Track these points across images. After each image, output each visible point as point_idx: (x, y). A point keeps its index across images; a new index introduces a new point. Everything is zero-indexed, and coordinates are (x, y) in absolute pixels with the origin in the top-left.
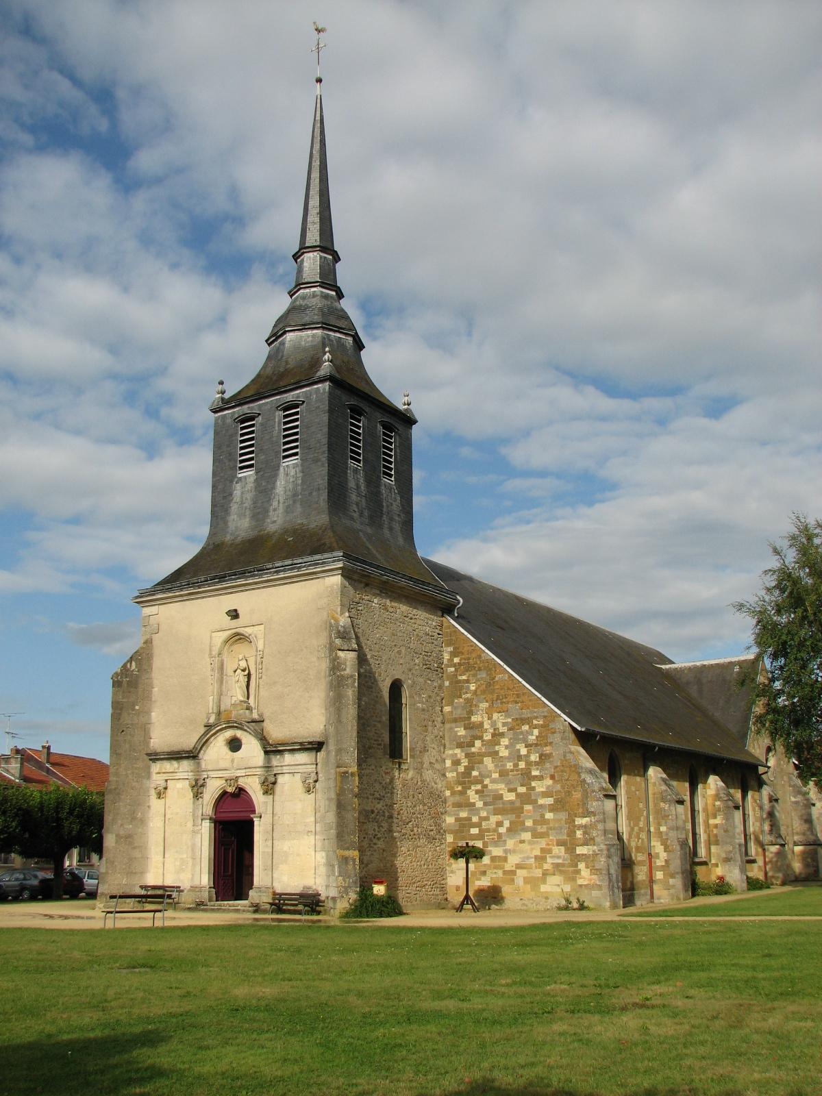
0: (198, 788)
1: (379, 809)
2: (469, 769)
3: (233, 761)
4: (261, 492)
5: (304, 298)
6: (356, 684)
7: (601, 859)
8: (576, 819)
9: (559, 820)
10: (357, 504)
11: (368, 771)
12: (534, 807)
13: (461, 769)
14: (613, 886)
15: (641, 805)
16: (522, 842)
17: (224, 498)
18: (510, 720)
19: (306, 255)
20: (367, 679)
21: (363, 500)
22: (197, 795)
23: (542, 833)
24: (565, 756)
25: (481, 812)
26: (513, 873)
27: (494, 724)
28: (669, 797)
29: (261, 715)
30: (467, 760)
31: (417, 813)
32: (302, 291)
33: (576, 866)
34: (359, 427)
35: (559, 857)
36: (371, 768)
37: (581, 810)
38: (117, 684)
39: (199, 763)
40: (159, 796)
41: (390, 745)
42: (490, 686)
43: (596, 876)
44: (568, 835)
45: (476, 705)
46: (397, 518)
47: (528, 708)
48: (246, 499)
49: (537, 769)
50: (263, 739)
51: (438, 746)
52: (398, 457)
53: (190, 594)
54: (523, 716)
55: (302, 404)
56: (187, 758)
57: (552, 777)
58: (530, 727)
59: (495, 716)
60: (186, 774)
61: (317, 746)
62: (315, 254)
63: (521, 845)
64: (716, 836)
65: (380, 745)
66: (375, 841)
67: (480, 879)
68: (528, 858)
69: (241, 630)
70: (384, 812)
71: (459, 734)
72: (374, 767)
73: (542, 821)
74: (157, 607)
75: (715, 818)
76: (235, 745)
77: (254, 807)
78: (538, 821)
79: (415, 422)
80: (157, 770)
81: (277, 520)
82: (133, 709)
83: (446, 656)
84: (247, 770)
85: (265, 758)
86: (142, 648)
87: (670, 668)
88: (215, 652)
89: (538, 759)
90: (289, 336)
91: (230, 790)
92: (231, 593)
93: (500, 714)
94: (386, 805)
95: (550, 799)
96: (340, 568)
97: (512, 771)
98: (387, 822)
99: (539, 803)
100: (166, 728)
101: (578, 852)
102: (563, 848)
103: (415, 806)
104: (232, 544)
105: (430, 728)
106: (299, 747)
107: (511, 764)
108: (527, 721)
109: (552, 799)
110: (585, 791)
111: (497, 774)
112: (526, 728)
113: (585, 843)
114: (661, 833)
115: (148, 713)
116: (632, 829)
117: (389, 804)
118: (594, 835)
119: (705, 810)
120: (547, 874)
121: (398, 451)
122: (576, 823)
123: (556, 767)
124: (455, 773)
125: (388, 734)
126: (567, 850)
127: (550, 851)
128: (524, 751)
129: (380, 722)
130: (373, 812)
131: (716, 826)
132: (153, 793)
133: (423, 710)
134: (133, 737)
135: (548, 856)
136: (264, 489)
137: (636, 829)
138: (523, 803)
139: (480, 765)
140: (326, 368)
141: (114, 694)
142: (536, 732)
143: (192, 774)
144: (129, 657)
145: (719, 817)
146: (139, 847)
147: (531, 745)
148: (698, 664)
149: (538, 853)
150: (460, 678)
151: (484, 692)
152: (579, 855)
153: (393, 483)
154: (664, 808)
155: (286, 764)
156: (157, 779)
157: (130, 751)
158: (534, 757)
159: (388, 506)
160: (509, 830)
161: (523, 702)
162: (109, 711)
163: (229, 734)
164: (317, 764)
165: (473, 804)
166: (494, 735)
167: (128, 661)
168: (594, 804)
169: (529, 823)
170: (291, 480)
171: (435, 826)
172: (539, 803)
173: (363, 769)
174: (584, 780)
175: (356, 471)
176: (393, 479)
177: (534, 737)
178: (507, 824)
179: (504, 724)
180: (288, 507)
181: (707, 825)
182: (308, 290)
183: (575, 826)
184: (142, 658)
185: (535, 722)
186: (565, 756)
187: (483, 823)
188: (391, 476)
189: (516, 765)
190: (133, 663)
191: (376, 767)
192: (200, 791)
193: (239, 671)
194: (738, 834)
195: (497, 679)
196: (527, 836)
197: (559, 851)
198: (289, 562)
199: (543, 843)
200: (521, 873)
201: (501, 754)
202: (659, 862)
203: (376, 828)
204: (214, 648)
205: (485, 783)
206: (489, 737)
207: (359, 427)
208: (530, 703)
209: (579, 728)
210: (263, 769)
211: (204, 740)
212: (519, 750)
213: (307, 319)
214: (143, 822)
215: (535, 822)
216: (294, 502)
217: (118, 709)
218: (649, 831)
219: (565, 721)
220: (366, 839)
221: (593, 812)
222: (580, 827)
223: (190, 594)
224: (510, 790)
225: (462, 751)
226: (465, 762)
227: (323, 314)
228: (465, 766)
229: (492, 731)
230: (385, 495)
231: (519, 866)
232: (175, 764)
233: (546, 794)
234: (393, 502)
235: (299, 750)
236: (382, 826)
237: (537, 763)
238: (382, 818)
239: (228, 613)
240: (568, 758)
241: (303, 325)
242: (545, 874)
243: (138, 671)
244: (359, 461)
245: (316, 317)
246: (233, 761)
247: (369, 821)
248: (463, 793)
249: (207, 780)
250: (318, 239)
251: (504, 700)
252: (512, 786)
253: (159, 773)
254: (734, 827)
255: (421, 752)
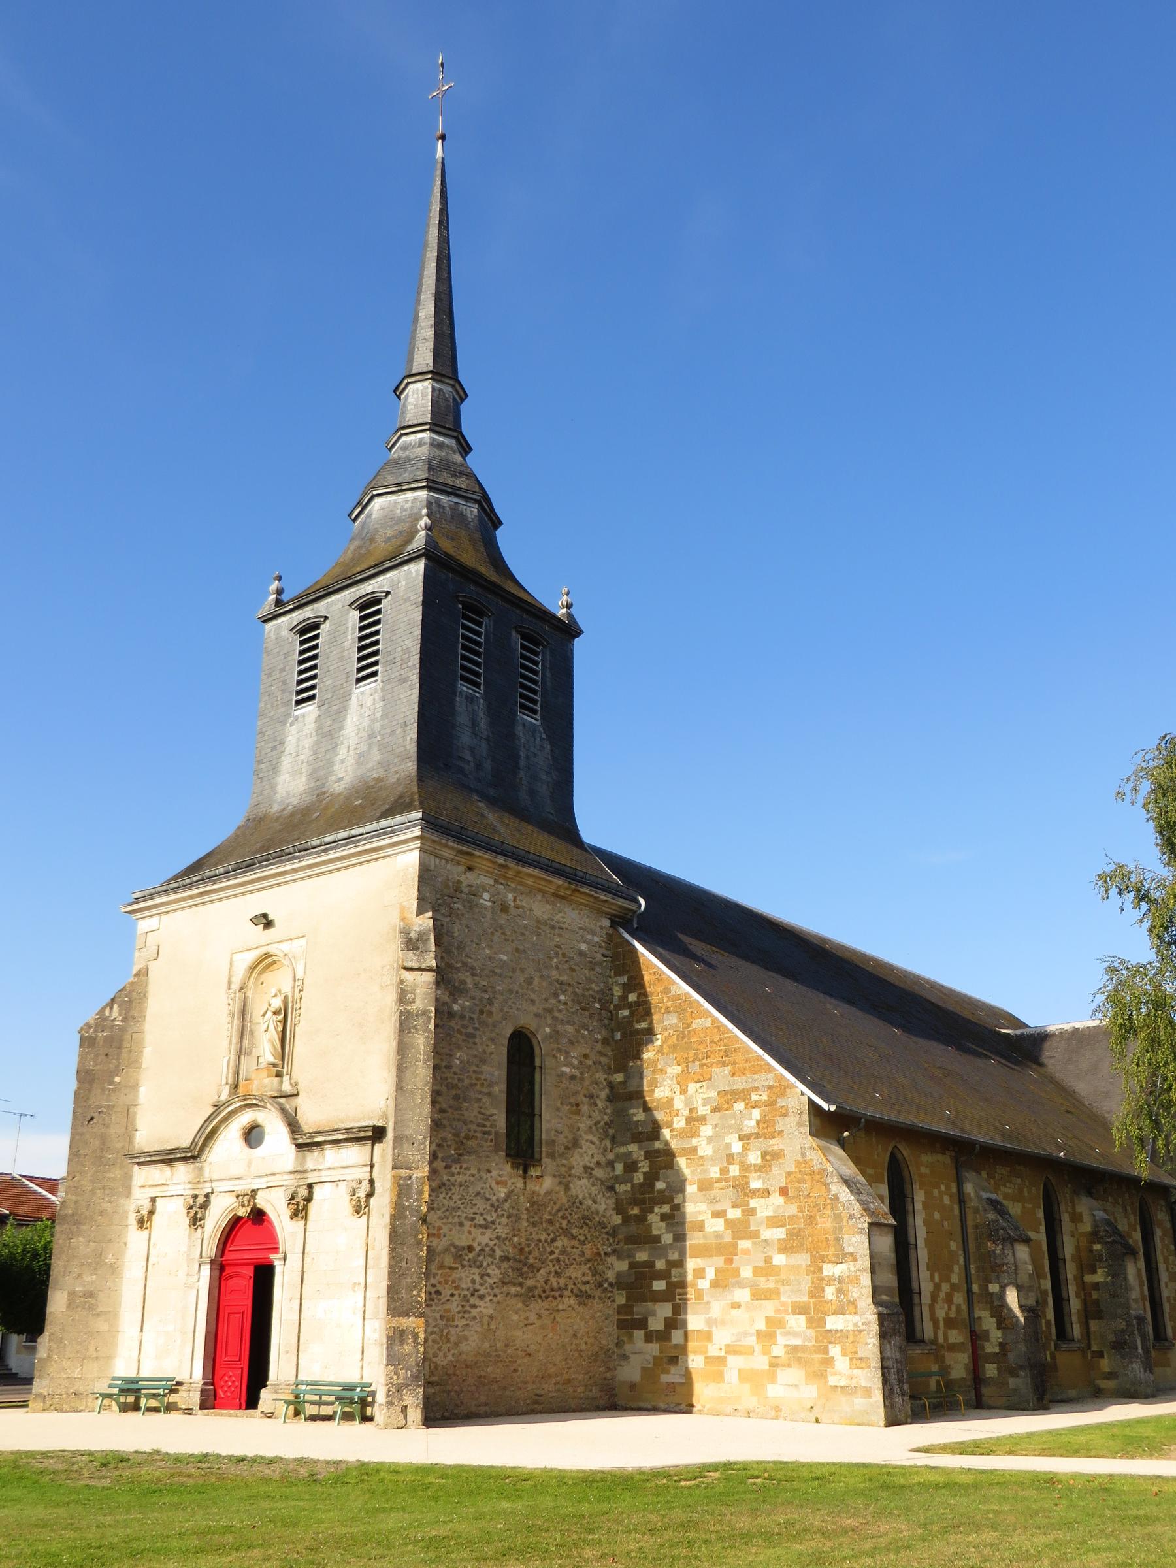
0: (197, 1213)
1: (483, 1244)
2: (651, 1178)
3: (249, 1164)
4: (324, 735)
5: (405, 448)
6: (432, 1026)
7: (869, 1341)
8: (825, 1266)
9: (795, 1268)
10: (472, 750)
11: (460, 1178)
12: (754, 1243)
13: (639, 1178)
14: (891, 1391)
15: (953, 1246)
16: (736, 1306)
17: (274, 748)
18: (714, 1094)
19: (411, 386)
20: (466, 1022)
21: (484, 745)
22: (196, 1221)
23: (769, 1290)
24: (803, 1155)
25: (670, 1252)
26: (721, 1360)
27: (688, 1102)
28: (1001, 1232)
29: (294, 1085)
30: (647, 1163)
31: (557, 1252)
32: (404, 439)
33: (826, 1350)
34: (479, 634)
35: (796, 1335)
36: (469, 1173)
37: (831, 1251)
38: (87, 1041)
39: (201, 1169)
40: (141, 1223)
41: (508, 1135)
42: (683, 1038)
43: (859, 1371)
44: (812, 1295)
45: (661, 1070)
46: (544, 777)
47: (743, 1074)
48: (304, 748)
49: (759, 1177)
50: (293, 1126)
51: (601, 1140)
52: (549, 684)
53: (202, 894)
54: (735, 1087)
55: (386, 596)
56: (185, 1159)
57: (784, 1192)
58: (747, 1105)
59: (692, 1087)
60: (182, 1187)
61: (377, 1134)
62: (426, 383)
63: (734, 1312)
64: (1096, 1302)
65: (489, 1133)
66: (473, 1301)
67: (668, 1372)
68: (746, 1334)
69: (272, 949)
70: (493, 1251)
71: (635, 1119)
72: (475, 1172)
73: (768, 1269)
74: (157, 918)
75: (1094, 1272)
76: (252, 1135)
77: (277, 1243)
78: (761, 1268)
79: (579, 633)
80: (140, 1184)
81: (345, 772)
82: (111, 1082)
83: (617, 991)
84: (270, 1178)
85: (297, 1157)
86: (132, 983)
87: (1023, 1034)
88: (235, 986)
89: (759, 1161)
90: (377, 503)
91: (243, 1212)
92: (262, 889)
93: (699, 1085)
94: (498, 1238)
95: (781, 1229)
96: (417, 838)
97: (718, 1181)
98: (499, 1268)
99: (763, 1237)
100: (161, 1108)
101: (828, 1327)
102: (803, 1318)
103: (553, 1240)
104: (278, 818)
105: (585, 1108)
106: (345, 1136)
107: (717, 1169)
108: (742, 1095)
109: (783, 1230)
110: (837, 1217)
111: (695, 1187)
112: (740, 1106)
113: (840, 1311)
114: (992, 1294)
115: (135, 1087)
116: (937, 1287)
117: (504, 1236)
118: (855, 1295)
119: (1077, 1258)
120: (777, 1365)
121: (548, 674)
122: (825, 1273)
123: (789, 1174)
124: (629, 1185)
125: (504, 1115)
126: (810, 1321)
127: (781, 1323)
128: (737, 1147)
129: (489, 1094)
130: (470, 1249)
131: (1096, 1286)
132: (132, 1220)
133: (573, 1077)
134: (108, 1127)
135: (778, 1331)
136: (328, 735)
137: (945, 1287)
138: (737, 1236)
139: (669, 1172)
140: (419, 541)
141: (83, 1058)
142: (756, 1114)
143: (190, 1186)
144: (108, 1000)
145: (1100, 1271)
146: (106, 1313)
147: (748, 1137)
148: (1067, 1027)
149: (761, 1325)
150: (637, 1026)
151: (674, 1048)
152: (830, 1331)
153: (539, 723)
154: (993, 1251)
155: (327, 1165)
156: (140, 1198)
157: (102, 1150)
158: (754, 1158)
159: (528, 757)
160: (715, 1284)
161: (735, 1063)
162: (72, 1084)
163: (245, 1119)
164: (372, 1166)
165: (657, 1239)
166: (689, 1120)
167: (107, 1005)
168: (854, 1239)
169: (746, 1273)
170: (367, 714)
171: (593, 1275)
172: (763, 1237)
173: (453, 1175)
174: (836, 1198)
175: (470, 699)
176: (538, 717)
177: (753, 1123)
178: (710, 1274)
179: (706, 1101)
180: (360, 755)
181: (1082, 1285)
182: (412, 437)
183: (823, 1279)
184: (130, 999)
185: (755, 1097)
186: (803, 1155)
187: (673, 1272)
188: (535, 712)
189: (724, 1171)
190: (116, 1006)
191: (479, 1170)
192: (199, 1215)
193: (269, 1014)
194: (1136, 1301)
195: (694, 1026)
196: (742, 1295)
197: (798, 1323)
198: (344, 834)
199: (769, 1308)
200: (734, 1362)
201: (700, 1153)
202: (991, 1348)
203: (477, 1278)
204: (233, 979)
205: (676, 1202)
206: (683, 1124)
207: (479, 634)
208: (747, 1065)
209: (825, 1106)
210: (293, 1176)
211: (210, 1128)
212: (729, 1145)
213: (406, 476)
214: (114, 1269)
215: (757, 1271)
216: (370, 746)
217: (87, 1078)
218: (969, 1291)
219: (802, 1094)
220: (456, 1298)
221: (852, 1254)
222: (831, 1280)
223: (202, 894)
224: (717, 1215)
225: (640, 1148)
226: (644, 1166)
227: (431, 468)
228: (645, 1173)
229: (686, 1113)
230: (523, 740)
231: (731, 1350)
232: (166, 1168)
233: (774, 1222)
234: (539, 754)
235: (347, 1140)
236: (488, 1275)
237: (759, 1169)
238: (490, 1260)
239: (254, 920)
240: (808, 1158)
241: (400, 484)
242: (774, 1364)
243: (122, 1021)
244: (477, 685)
245: (419, 473)
246: (249, 1164)
247: (463, 1266)
248: (641, 1219)
249: (212, 1197)
250: (430, 361)
251: (705, 1061)
252: (718, 1207)
253: (144, 1187)
254: (1128, 1289)
255: (567, 1148)
